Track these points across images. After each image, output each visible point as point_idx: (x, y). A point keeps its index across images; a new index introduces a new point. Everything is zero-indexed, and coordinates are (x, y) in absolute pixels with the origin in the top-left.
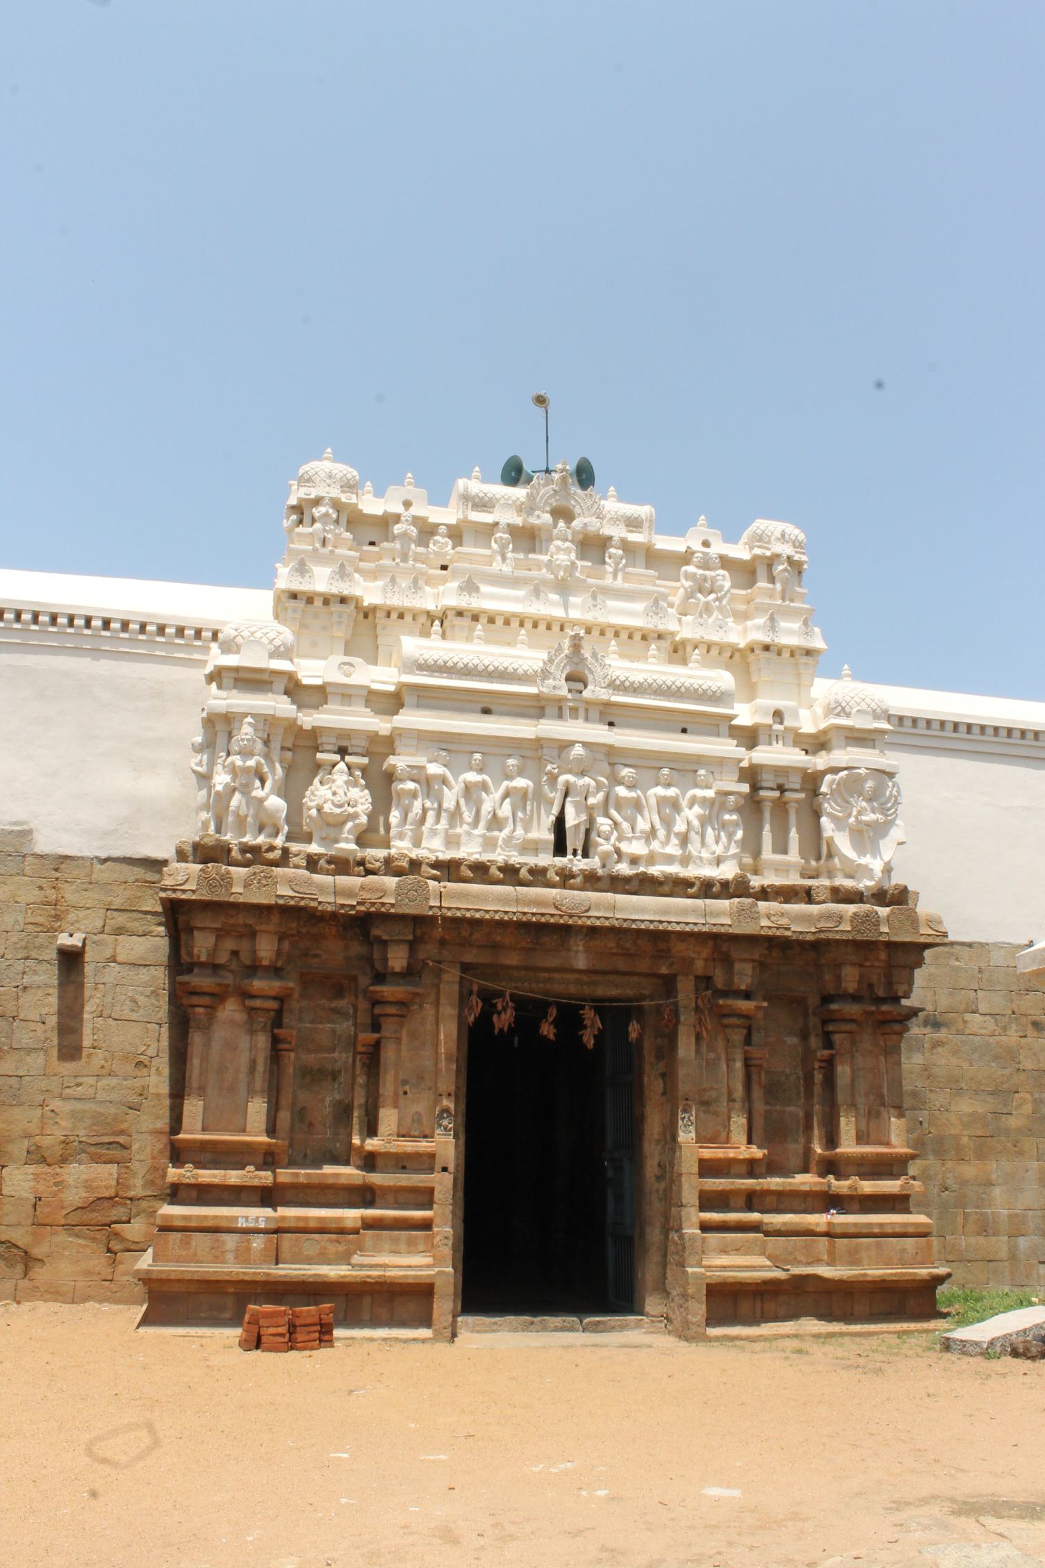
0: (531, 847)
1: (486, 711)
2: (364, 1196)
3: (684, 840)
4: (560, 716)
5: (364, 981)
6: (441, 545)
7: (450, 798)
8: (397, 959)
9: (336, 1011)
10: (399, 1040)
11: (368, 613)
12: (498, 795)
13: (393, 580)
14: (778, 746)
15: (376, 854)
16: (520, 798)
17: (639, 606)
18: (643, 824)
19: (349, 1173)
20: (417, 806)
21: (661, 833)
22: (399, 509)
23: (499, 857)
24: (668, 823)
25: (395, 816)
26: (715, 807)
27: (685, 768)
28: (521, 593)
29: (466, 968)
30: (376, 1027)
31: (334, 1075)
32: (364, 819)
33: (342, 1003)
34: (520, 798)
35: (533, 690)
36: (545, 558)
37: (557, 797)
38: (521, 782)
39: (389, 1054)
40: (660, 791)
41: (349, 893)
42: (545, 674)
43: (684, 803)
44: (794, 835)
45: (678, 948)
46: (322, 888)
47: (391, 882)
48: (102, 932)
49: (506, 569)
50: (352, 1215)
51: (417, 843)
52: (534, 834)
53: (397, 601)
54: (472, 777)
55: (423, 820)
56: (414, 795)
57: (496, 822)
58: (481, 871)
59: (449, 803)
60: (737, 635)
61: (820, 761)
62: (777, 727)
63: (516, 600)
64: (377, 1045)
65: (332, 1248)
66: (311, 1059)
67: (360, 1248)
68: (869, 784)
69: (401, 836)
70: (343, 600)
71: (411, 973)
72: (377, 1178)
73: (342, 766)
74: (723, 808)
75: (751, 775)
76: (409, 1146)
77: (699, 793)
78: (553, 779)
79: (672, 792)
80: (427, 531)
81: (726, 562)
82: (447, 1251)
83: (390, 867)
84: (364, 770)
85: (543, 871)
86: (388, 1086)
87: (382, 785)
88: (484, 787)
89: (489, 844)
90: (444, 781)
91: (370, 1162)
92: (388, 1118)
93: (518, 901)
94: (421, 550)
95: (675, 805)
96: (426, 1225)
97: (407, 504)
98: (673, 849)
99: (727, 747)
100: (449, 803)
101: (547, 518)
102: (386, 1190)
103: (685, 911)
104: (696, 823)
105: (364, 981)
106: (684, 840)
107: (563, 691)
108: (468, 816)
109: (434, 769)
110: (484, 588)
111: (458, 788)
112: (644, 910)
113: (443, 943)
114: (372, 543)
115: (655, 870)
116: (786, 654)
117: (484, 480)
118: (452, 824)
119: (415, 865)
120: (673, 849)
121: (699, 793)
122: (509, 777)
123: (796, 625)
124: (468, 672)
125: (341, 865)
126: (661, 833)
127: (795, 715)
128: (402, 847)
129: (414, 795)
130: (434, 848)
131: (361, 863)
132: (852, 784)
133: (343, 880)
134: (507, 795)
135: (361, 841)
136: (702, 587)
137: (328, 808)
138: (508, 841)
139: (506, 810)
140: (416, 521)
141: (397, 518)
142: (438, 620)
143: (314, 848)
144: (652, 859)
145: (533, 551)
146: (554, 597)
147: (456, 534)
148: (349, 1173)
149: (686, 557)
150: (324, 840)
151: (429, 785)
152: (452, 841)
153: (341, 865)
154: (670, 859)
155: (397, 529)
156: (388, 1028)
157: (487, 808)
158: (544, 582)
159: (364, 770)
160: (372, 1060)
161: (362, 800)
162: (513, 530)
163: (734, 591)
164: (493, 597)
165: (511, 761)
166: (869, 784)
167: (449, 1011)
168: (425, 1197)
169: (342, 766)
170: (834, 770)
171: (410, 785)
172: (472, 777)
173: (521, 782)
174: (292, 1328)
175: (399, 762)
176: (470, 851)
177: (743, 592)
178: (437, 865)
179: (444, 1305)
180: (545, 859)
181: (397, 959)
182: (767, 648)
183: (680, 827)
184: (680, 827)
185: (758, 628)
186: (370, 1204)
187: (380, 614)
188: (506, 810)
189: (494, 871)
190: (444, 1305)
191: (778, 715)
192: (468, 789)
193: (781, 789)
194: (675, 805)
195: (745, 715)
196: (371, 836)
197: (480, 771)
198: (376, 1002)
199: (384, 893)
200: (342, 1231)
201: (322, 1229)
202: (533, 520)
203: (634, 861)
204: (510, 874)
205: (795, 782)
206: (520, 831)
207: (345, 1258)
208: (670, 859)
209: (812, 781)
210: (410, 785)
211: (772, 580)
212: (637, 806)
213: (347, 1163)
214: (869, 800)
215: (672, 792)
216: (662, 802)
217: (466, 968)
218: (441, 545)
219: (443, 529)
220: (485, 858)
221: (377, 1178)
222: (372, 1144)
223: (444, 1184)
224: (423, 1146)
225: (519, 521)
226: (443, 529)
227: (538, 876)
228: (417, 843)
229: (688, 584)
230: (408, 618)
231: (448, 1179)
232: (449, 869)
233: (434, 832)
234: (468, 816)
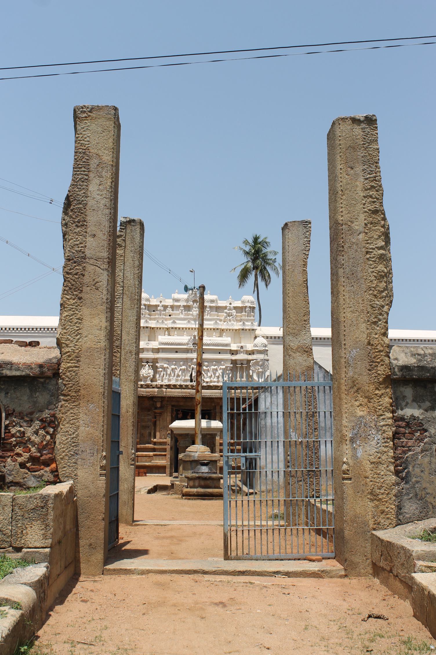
0: (185, 381)
1: (177, 352)
2: (154, 450)
3: (218, 377)
4: (192, 353)
5: (153, 409)
6: (169, 310)
7: (169, 371)
8: (159, 405)
9: (148, 414)
10: (160, 420)
11: (153, 328)
12: (179, 370)
13: (158, 321)
14: (242, 354)
15: (154, 383)
16: (183, 371)
17: (212, 322)
18: (209, 374)
19: (151, 446)
20: (162, 373)
21: (213, 376)
22: (158, 303)
23: (179, 383)
24: (215, 374)
25: (158, 376)
26: (224, 370)
27: (219, 362)
28: (186, 322)
29: (173, 406)
30: (155, 418)
31: (148, 427)
32: (152, 376)
33: (149, 413)
34: (183, 371)
35: (185, 347)
36: (191, 313)
37: (191, 370)
38: (183, 367)
39: (158, 423)
40: (213, 367)
41: (149, 392)
42: (187, 344)
43: (218, 369)
44: (245, 374)
45: (216, 400)
46: (143, 392)
47: (156, 390)
48: (273, 529)
49: (182, 316)
50: (151, 454)
51: (162, 381)
52: (186, 378)
53: (158, 326)
54: (173, 367)
55: (163, 376)
56: (161, 371)
57: (178, 376)
58: (175, 387)
59: (169, 373)
60: (238, 326)
61: (250, 357)
62: (242, 350)
63: (184, 324)
64: (156, 422)
65: (148, 460)
66: (144, 424)
67: (153, 460)
68: (261, 363)
69: (159, 380)
70: (147, 327)
71: (162, 407)
72: (156, 447)
73: (147, 366)
74: (227, 370)
75: (234, 362)
76: (162, 440)
77: (222, 367)
78: (190, 366)
79: (215, 367)
80: (165, 307)
81: (235, 308)
82: (169, 460)
83: (156, 386)
84: (152, 366)
85: (188, 385)
86: (158, 429)
87: (155, 368)
88: (176, 368)
89: (177, 380)
90: (168, 368)
91: (155, 444)
92: (158, 434)
93: (181, 393)
94: (164, 312)
95: (216, 370)
96: (165, 455)
97: (161, 302)
98: (216, 380)
99: (228, 356)
100: (169, 373)
101: (192, 303)
102: (158, 449)
103: (216, 393)
104: (221, 374)
105: (153, 409)
106: (218, 377)
107: (192, 347)
108: (173, 375)
109: (165, 366)
110: (177, 322)
111: (170, 369)
112: (207, 393)
113: (168, 401)
114: (154, 311)
115: (211, 384)
116: (248, 330)
117: (178, 293)
118: (169, 377)
119: (162, 386)
120: (216, 380)
121: (222, 367)
122: (181, 366)
123: (250, 323)
124: (172, 344)
125: (148, 386)
126: (213, 376)
127: (246, 346)
128: (159, 382)
129: (161, 371)
130: (166, 382)
131: (152, 385)
132: (257, 363)
133: (148, 390)
134: (181, 370)
135: (152, 381)
136: (229, 315)
137: (144, 375)
138: (181, 380)
139: (180, 373)
140: (163, 306)
141: (159, 306)
142: (168, 330)
143: (142, 383)
144: (211, 382)
145: (189, 311)
146: (193, 322)
147: (172, 307)
148: (151, 446)
149: (225, 308)
150: (145, 381)
151: (164, 369)
152: (169, 380)
153: (148, 386)
154: (214, 382)
155: (159, 308)
156: (158, 418)
157: (176, 373)
158: (191, 319)
159: (152, 366)
160: (155, 424)
161: (151, 372)
162: (184, 306)
163: (237, 314)
164: (179, 324)
165: (181, 363)
166: (261, 363)
167: (169, 414)
168: (165, 450)
169: (147, 366)
170: (253, 360)
171: (161, 369)
172: (173, 367)
173: (183, 367)
174: (139, 473)
175: (158, 365)
176: (173, 382)
177: (240, 314)
178: (166, 385)
179: (168, 470)
180: (189, 383)
181: (159, 405)
182: (243, 329)
183: (217, 375)
184: (217, 375)
185: (240, 325)
186: (155, 452)
187: (156, 329)
188: (180, 373)
189: (178, 386)
190: (168, 470)
191: (242, 347)
192: (172, 369)
193: (242, 364)
194: (216, 370)
195: (234, 347)
196: (154, 379)
197: (175, 365)
198: (155, 413)
199: (155, 392)
200: (150, 457)
201: (146, 456)
202: (188, 304)
203: (207, 382)
204: (181, 387)
205: (245, 362)
206: (183, 377)
207: (150, 461)
208: (214, 382)
209: (249, 361)
210: (161, 369)
211: (245, 312)
212: (208, 370)
213: (151, 444)
214: (261, 366)
215: (215, 367)
216: (213, 369)
217: (173, 406)
218: (169, 310)
219: (169, 306)
220: (176, 383)
221: (156, 447)
222: (155, 440)
223: (168, 447)
224: (165, 440)
225: (185, 304)
226: (169, 306)
227: (187, 387)
228: (162, 381)
229: (225, 315)
230: (162, 329)
231: (169, 447)
232: (168, 386)
233: (165, 379)
234: (173, 375)
